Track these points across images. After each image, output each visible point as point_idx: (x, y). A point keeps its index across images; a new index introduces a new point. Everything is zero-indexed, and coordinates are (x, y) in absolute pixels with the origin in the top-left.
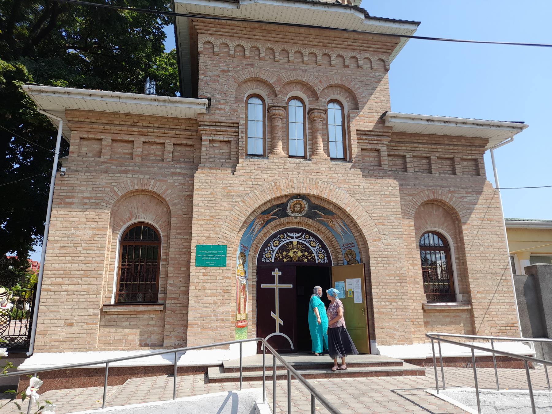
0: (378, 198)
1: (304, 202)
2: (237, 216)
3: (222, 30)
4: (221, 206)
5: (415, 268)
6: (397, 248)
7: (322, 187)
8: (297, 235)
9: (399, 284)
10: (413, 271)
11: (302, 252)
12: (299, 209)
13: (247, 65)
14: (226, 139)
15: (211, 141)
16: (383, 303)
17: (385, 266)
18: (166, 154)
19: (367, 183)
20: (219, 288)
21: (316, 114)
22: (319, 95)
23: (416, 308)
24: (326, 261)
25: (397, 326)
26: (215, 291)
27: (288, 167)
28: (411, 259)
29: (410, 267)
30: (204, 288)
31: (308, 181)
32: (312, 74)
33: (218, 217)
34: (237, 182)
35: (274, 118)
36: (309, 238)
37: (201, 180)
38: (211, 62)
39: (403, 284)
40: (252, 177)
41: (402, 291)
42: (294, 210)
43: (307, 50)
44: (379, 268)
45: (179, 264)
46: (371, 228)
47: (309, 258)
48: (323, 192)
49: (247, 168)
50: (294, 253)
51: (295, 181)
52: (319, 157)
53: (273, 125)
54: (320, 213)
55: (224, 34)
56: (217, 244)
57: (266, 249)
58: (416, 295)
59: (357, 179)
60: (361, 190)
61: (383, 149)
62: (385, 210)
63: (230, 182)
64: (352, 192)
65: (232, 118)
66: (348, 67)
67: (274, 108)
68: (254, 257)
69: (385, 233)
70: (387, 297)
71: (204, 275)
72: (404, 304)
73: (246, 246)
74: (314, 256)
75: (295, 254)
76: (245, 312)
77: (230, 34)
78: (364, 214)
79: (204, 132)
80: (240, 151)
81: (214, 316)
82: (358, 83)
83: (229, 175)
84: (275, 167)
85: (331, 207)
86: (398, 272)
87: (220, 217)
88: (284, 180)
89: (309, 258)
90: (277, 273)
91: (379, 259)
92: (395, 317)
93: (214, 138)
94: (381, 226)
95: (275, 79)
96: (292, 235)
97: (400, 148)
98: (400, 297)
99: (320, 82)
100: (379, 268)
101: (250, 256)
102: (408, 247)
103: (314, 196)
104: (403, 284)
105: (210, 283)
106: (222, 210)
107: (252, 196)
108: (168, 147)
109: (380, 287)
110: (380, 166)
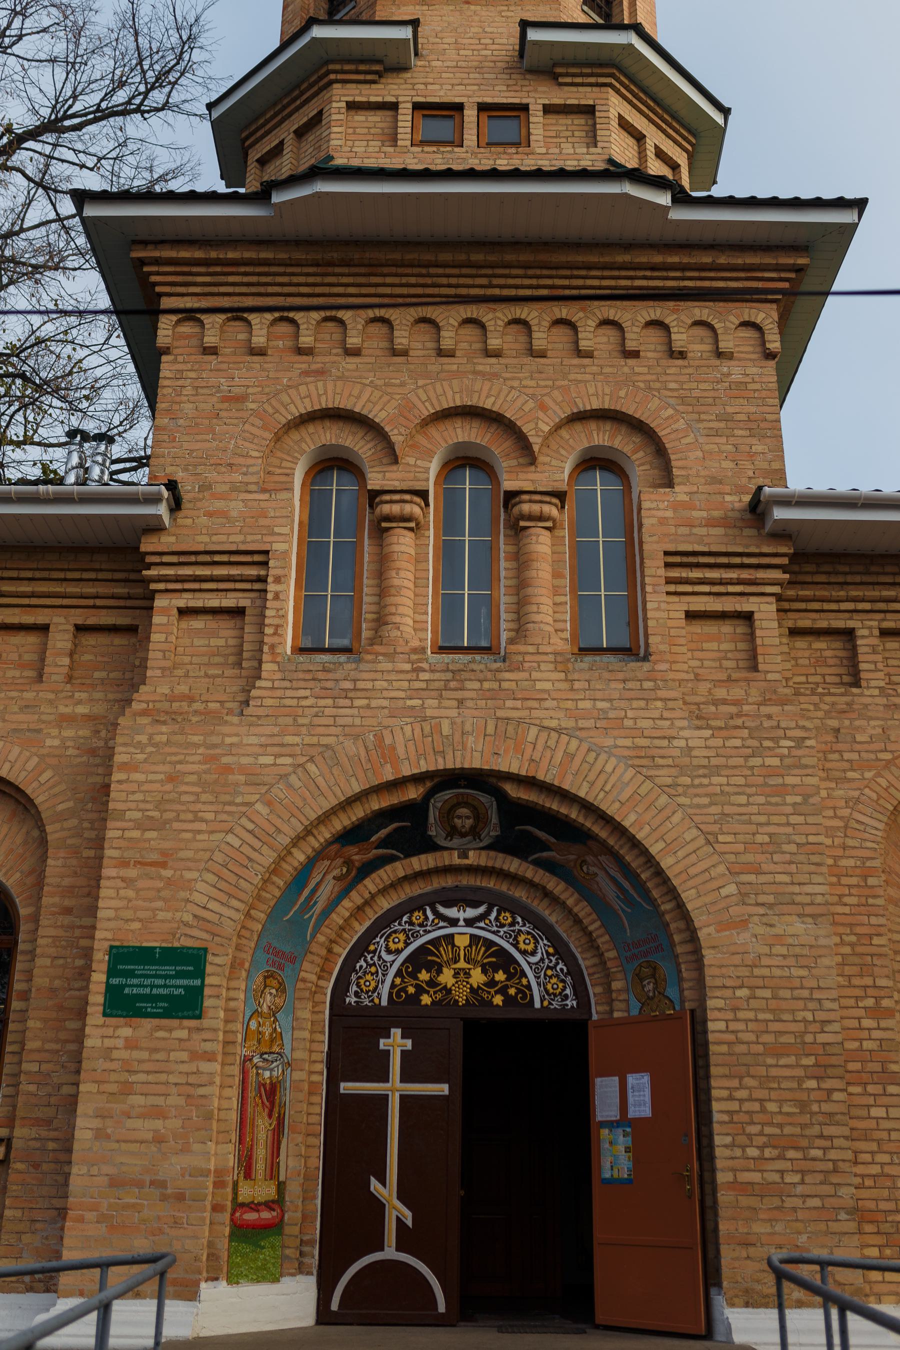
0: (742, 781)
1: (484, 799)
2: (246, 849)
3: (231, 279)
4: (197, 819)
5: (883, 1024)
6: (806, 951)
7: (540, 747)
8: (471, 913)
9: (813, 1084)
10: (876, 1034)
11: (484, 971)
12: (469, 823)
13: (306, 373)
14: (229, 601)
15: (183, 612)
16: (753, 1152)
17: (761, 1016)
18: (49, 660)
19: (699, 728)
20: (174, 1090)
21: (526, 508)
22: (536, 448)
23: (888, 1170)
24: (571, 1003)
25: (803, 1238)
26: (159, 1101)
27: (423, 685)
28: (870, 992)
29: (867, 1023)
30: (127, 1089)
31: (490, 729)
32: (516, 383)
33: (182, 854)
34: (254, 740)
35: (388, 529)
36: (513, 924)
37: (138, 738)
38: (192, 375)
39: (828, 1084)
40: (301, 721)
41: (826, 1107)
42: (454, 828)
43: (499, 314)
44: (741, 1026)
45: (60, 1008)
46: (714, 884)
47: (512, 991)
48: (544, 764)
49: (289, 693)
50: (456, 974)
51: (446, 729)
52: (531, 649)
53: (386, 550)
55: (238, 290)
56: (176, 944)
57: (362, 963)
58: (885, 1124)
59: (666, 714)
60: (677, 753)
61: (765, 610)
62: (763, 819)
63: (228, 740)
64: (644, 760)
65: (249, 538)
66: (635, 354)
67: (387, 497)
68: (320, 990)
69: (762, 899)
70: (768, 1130)
71: (131, 1045)
72: (833, 1155)
73: (287, 949)
74: (529, 987)
75: (462, 980)
76: (273, 1171)
77: (253, 290)
78: (688, 836)
79: (161, 586)
80: (266, 639)
81: (152, 1183)
82: (672, 401)
83: (228, 718)
84: (379, 684)
85: (574, 814)
86: (809, 1038)
87: (189, 854)
88: (408, 729)
89: (512, 991)
90: (396, 1043)
91: (740, 993)
92: (798, 1202)
93: (192, 604)
94: (752, 878)
95: (391, 408)
96: (452, 912)
97: (834, 606)
98: (816, 1130)
99: (543, 407)
100: (741, 1026)
101: (300, 985)
102: (860, 949)
104: (828, 1084)
105: (148, 1072)
106: (199, 832)
107: (297, 784)
108: (59, 636)
109: (742, 1094)
110: (755, 668)
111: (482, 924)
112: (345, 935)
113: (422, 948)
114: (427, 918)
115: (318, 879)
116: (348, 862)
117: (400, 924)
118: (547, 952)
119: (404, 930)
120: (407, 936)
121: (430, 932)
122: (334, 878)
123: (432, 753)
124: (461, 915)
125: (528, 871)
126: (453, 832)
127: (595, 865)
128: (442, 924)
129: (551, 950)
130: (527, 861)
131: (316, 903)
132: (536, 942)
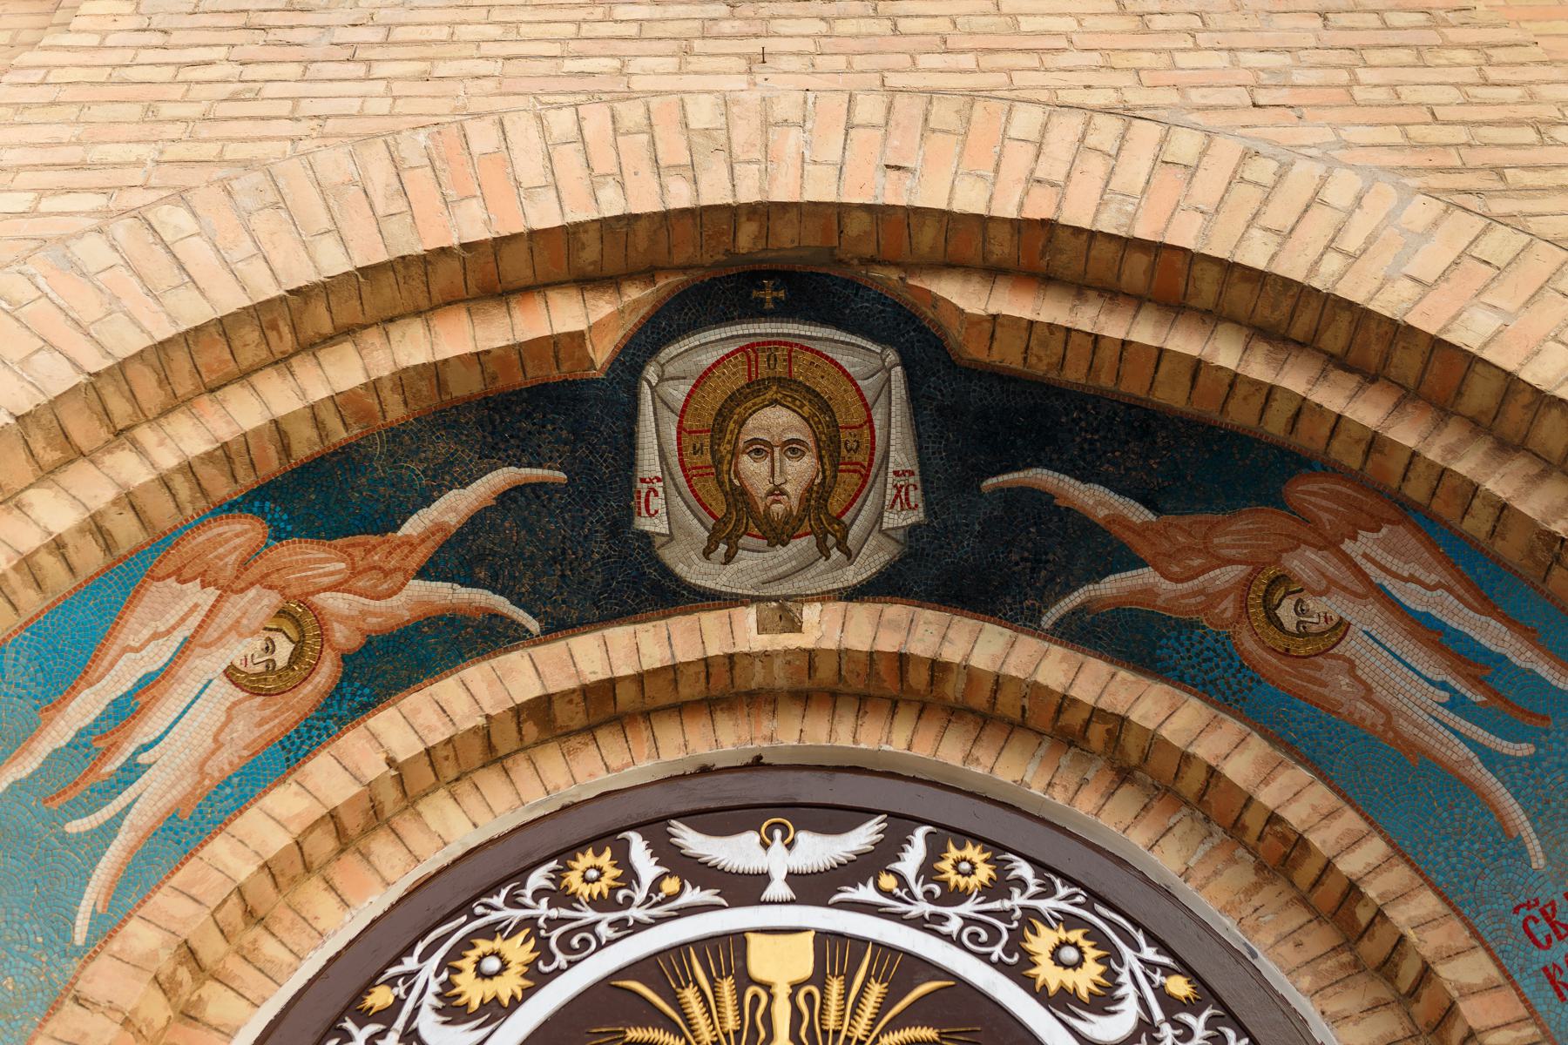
1: (860, 359)
8: (817, 851)
12: (800, 471)
36: (998, 887)
42: (739, 496)
54: (1094, 499)
96: (737, 852)
103: (971, 243)
111: (866, 893)
112: (270, 948)
113: (606, 986)
114: (629, 876)
115: (156, 656)
116: (296, 615)
117: (512, 901)
118: (1160, 992)
119: (532, 921)
120: (542, 944)
121: (640, 926)
122: (231, 673)
123: (646, 170)
124: (778, 861)
125: (1052, 667)
126: (736, 520)
127: (1330, 587)
128: (692, 896)
129: (1179, 986)
130: (1035, 630)
131: (132, 771)
132: (1110, 958)
